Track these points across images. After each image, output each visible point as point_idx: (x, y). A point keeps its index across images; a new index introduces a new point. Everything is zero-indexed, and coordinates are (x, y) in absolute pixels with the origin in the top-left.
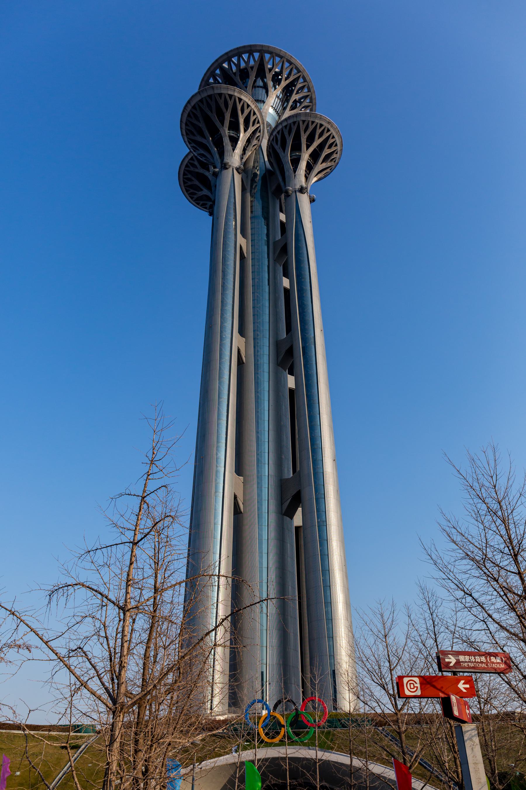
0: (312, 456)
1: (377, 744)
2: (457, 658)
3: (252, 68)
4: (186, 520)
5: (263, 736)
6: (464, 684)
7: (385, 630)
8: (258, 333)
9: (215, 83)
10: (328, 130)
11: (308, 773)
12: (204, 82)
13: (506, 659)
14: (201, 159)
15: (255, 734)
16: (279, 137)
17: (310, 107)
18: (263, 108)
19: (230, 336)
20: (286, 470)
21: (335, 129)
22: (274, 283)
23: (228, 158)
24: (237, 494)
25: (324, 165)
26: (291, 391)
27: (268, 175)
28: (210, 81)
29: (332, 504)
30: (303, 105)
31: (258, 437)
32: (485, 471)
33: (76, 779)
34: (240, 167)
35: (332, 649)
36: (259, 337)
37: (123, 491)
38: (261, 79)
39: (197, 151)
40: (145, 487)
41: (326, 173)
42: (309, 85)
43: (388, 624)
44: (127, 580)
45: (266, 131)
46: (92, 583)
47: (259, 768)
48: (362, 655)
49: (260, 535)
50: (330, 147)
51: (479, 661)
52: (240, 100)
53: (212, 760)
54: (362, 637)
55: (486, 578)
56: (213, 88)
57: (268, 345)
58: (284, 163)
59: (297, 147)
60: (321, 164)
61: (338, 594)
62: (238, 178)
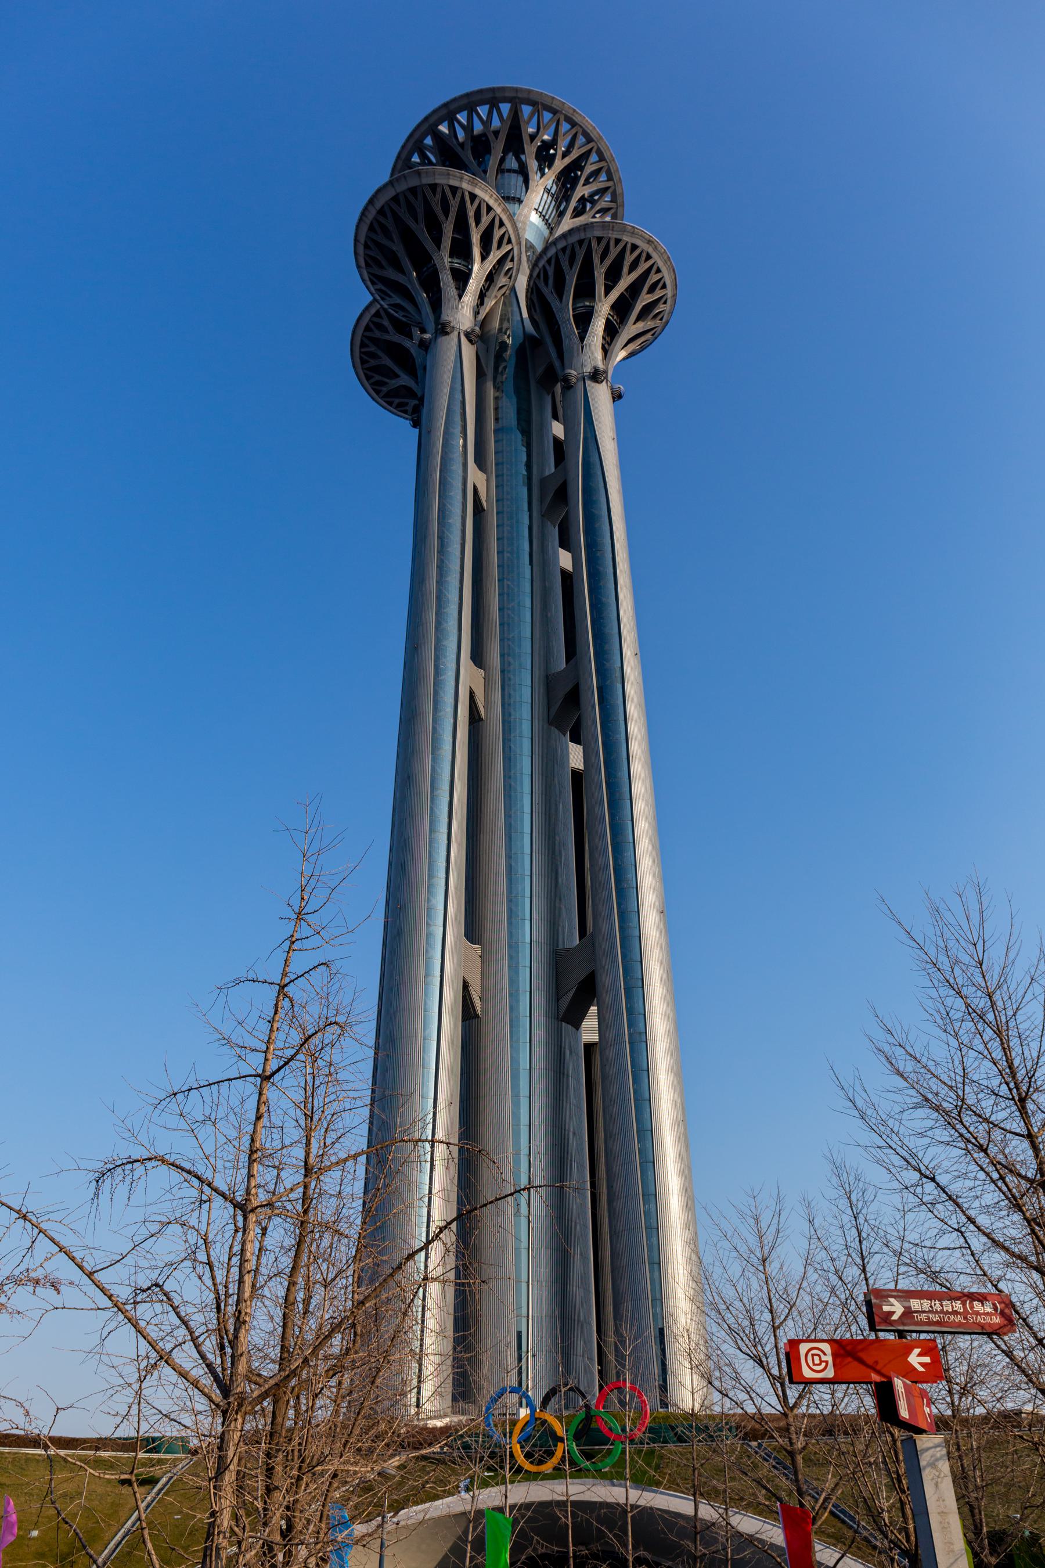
1: (747, 1474)
2: (906, 1304)
3: (496, 133)
4: (367, 1030)
5: (521, 1459)
6: (920, 1355)
7: (762, 1248)
8: (511, 660)
10: (649, 257)
11: (610, 1533)
12: (400, 163)
13: (1003, 1305)
15: (506, 1456)
16: (551, 271)
17: (612, 211)
19: (454, 666)
20: (566, 930)
22: (541, 561)
24: (468, 980)
25: (641, 326)
26: (576, 775)
27: (529, 347)
29: (657, 998)
30: (597, 207)
31: (511, 866)
32: (961, 932)
33: (150, 1546)
34: (473, 331)
35: (658, 1288)
37: (242, 974)
38: (513, 155)
40: (286, 965)
41: (643, 341)
43: (769, 1238)
44: (251, 1151)
46: (179, 1156)
48: (717, 1298)
49: (515, 1061)
50: (652, 290)
51: (950, 1310)
52: (473, 197)
53: (420, 1507)
54: (717, 1263)
55: (962, 1145)
56: (419, 173)
59: (586, 291)
60: (635, 323)
61: (670, 1177)
62: (469, 352)
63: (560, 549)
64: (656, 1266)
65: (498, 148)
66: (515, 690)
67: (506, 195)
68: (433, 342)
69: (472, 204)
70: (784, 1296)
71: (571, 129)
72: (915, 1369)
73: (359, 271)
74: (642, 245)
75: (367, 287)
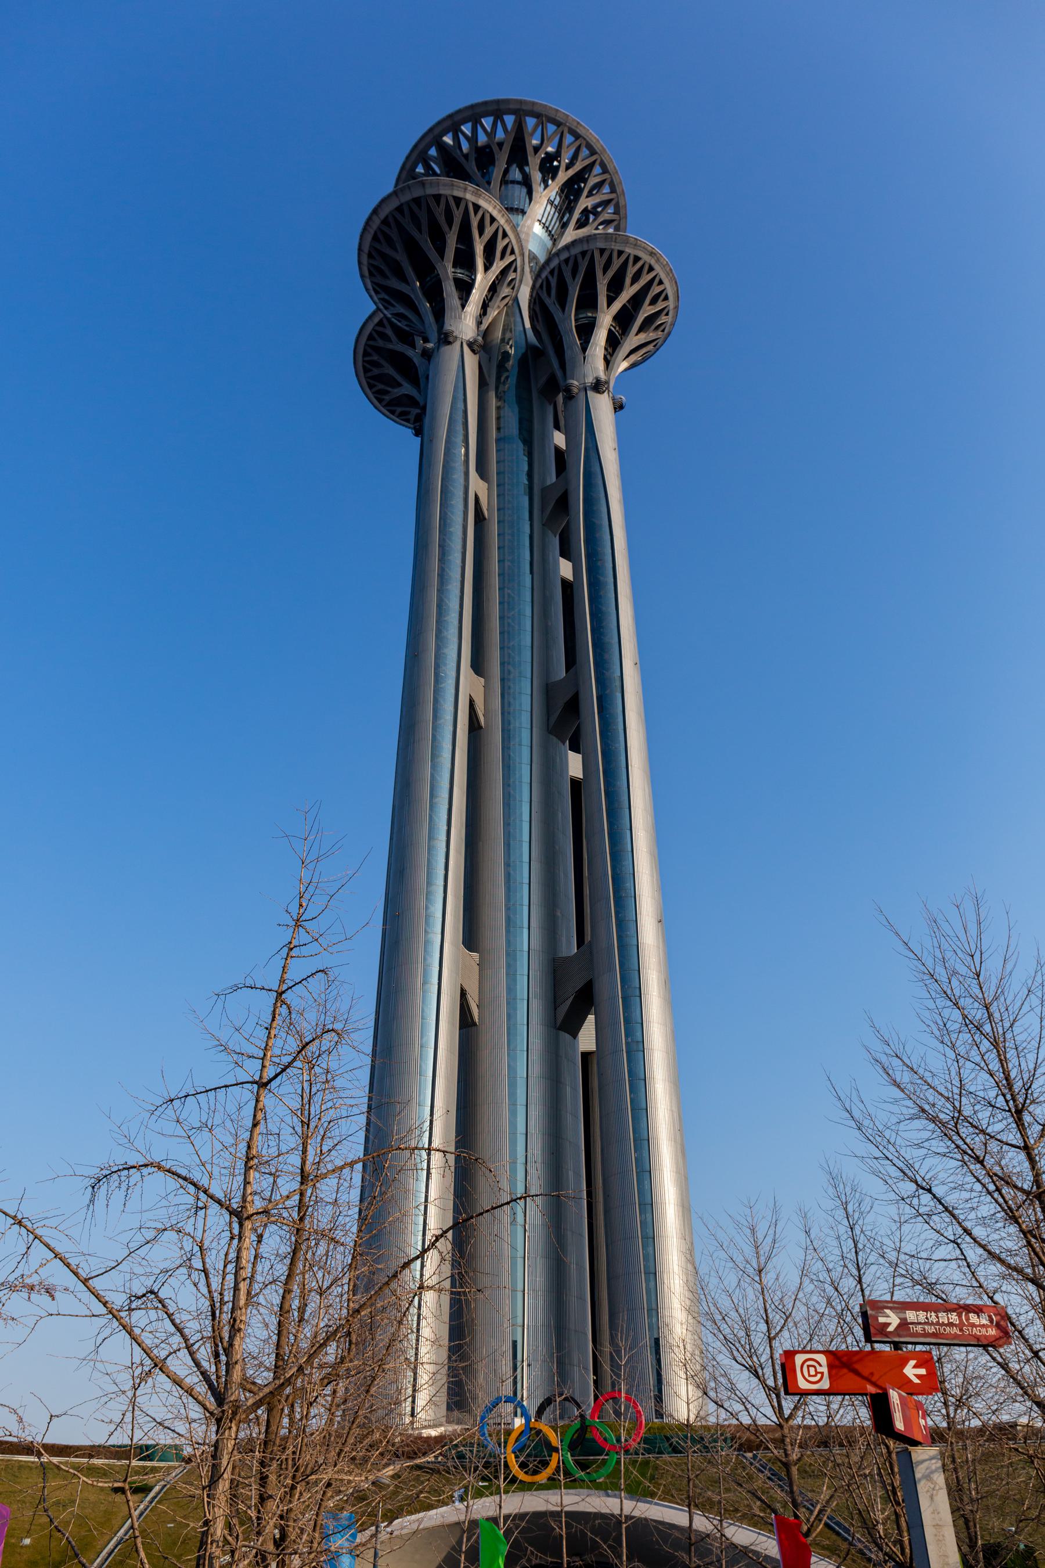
2: (902, 1316)
3: (500, 145)
4: (364, 1039)
5: (515, 1469)
6: (915, 1367)
7: (758, 1258)
8: (511, 669)
9: (426, 174)
10: (651, 269)
11: (605, 1543)
13: (999, 1317)
14: (399, 324)
15: (500, 1465)
17: (615, 223)
18: (521, 223)
19: (454, 674)
20: (564, 939)
21: (664, 267)
22: (542, 570)
24: (466, 987)
25: (643, 338)
26: (575, 784)
27: (531, 357)
28: (417, 170)
30: (601, 219)
32: (958, 943)
33: (142, 1554)
34: (475, 341)
35: (653, 1298)
36: (511, 677)
37: (239, 980)
38: (517, 166)
39: (392, 308)
41: (645, 352)
43: (765, 1248)
44: (247, 1158)
45: (527, 269)
47: (508, 1534)
48: (712, 1308)
49: (512, 1069)
50: (653, 301)
51: (946, 1322)
52: (477, 208)
53: (413, 1517)
54: (713, 1273)
55: (959, 1157)
56: (423, 184)
59: (588, 302)
60: (637, 335)
62: (471, 362)
64: (652, 1276)
65: (502, 159)
67: (510, 206)
72: (911, 1381)
74: (645, 257)
75: (371, 297)
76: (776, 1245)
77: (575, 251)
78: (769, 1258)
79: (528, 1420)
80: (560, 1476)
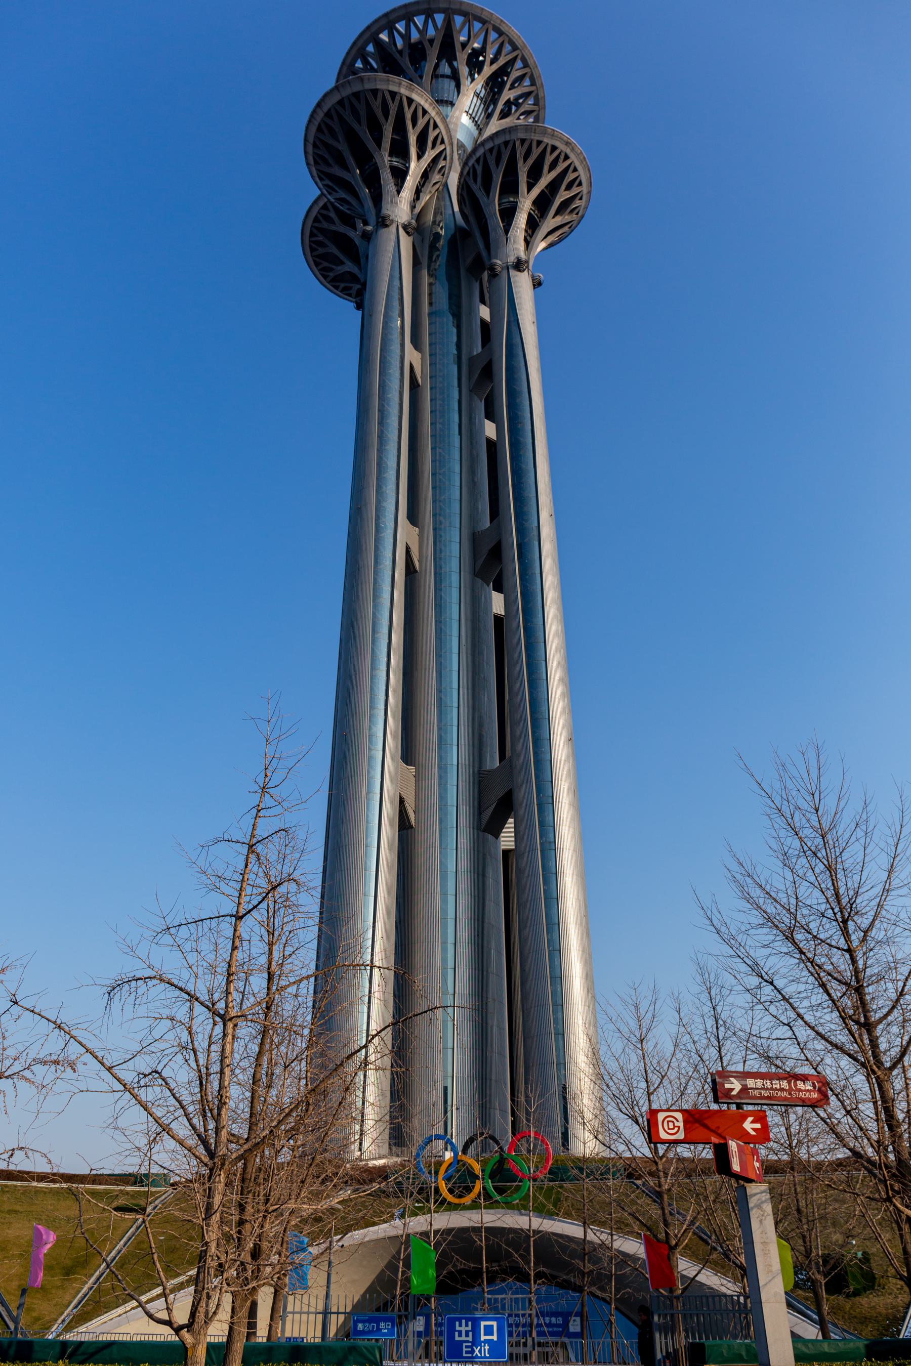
0: (533, 733)
1: (624, 1209)
2: (744, 1083)
3: (431, 41)
6: (752, 1122)
8: (442, 518)
9: (365, 70)
10: (567, 157)
12: (345, 68)
13: (820, 1084)
14: (341, 208)
15: (431, 1191)
16: (479, 170)
17: (535, 114)
18: (449, 114)
19: (392, 525)
20: (488, 755)
21: (578, 155)
22: (469, 431)
23: (389, 206)
24: (404, 796)
25: (559, 220)
26: (498, 620)
27: (460, 237)
28: (356, 65)
29: (565, 813)
30: (522, 110)
31: (441, 698)
32: (802, 784)
34: (410, 224)
35: (562, 1054)
36: (442, 526)
40: (254, 829)
41: (561, 233)
42: (532, 74)
43: (646, 1022)
44: (228, 974)
45: (456, 156)
47: (437, 1245)
48: (602, 1070)
49: (443, 865)
50: (569, 187)
51: (778, 1088)
52: (410, 101)
53: (362, 1231)
54: (603, 1042)
55: (798, 956)
56: (362, 79)
57: (458, 541)
58: (487, 216)
59: (510, 188)
60: (553, 217)
63: (487, 422)
64: (560, 1037)
66: (445, 546)
67: (440, 98)
68: (374, 234)
69: (409, 107)
70: (658, 1068)
71: (499, 37)
72: (749, 1133)
73: (309, 168)
74: (561, 146)
75: (316, 183)
76: (655, 1020)
77: (499, 141)
78: (649, 1030)
79: (456, 1154)
80: (480, 1199)
